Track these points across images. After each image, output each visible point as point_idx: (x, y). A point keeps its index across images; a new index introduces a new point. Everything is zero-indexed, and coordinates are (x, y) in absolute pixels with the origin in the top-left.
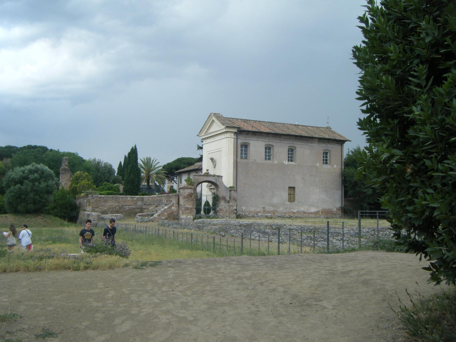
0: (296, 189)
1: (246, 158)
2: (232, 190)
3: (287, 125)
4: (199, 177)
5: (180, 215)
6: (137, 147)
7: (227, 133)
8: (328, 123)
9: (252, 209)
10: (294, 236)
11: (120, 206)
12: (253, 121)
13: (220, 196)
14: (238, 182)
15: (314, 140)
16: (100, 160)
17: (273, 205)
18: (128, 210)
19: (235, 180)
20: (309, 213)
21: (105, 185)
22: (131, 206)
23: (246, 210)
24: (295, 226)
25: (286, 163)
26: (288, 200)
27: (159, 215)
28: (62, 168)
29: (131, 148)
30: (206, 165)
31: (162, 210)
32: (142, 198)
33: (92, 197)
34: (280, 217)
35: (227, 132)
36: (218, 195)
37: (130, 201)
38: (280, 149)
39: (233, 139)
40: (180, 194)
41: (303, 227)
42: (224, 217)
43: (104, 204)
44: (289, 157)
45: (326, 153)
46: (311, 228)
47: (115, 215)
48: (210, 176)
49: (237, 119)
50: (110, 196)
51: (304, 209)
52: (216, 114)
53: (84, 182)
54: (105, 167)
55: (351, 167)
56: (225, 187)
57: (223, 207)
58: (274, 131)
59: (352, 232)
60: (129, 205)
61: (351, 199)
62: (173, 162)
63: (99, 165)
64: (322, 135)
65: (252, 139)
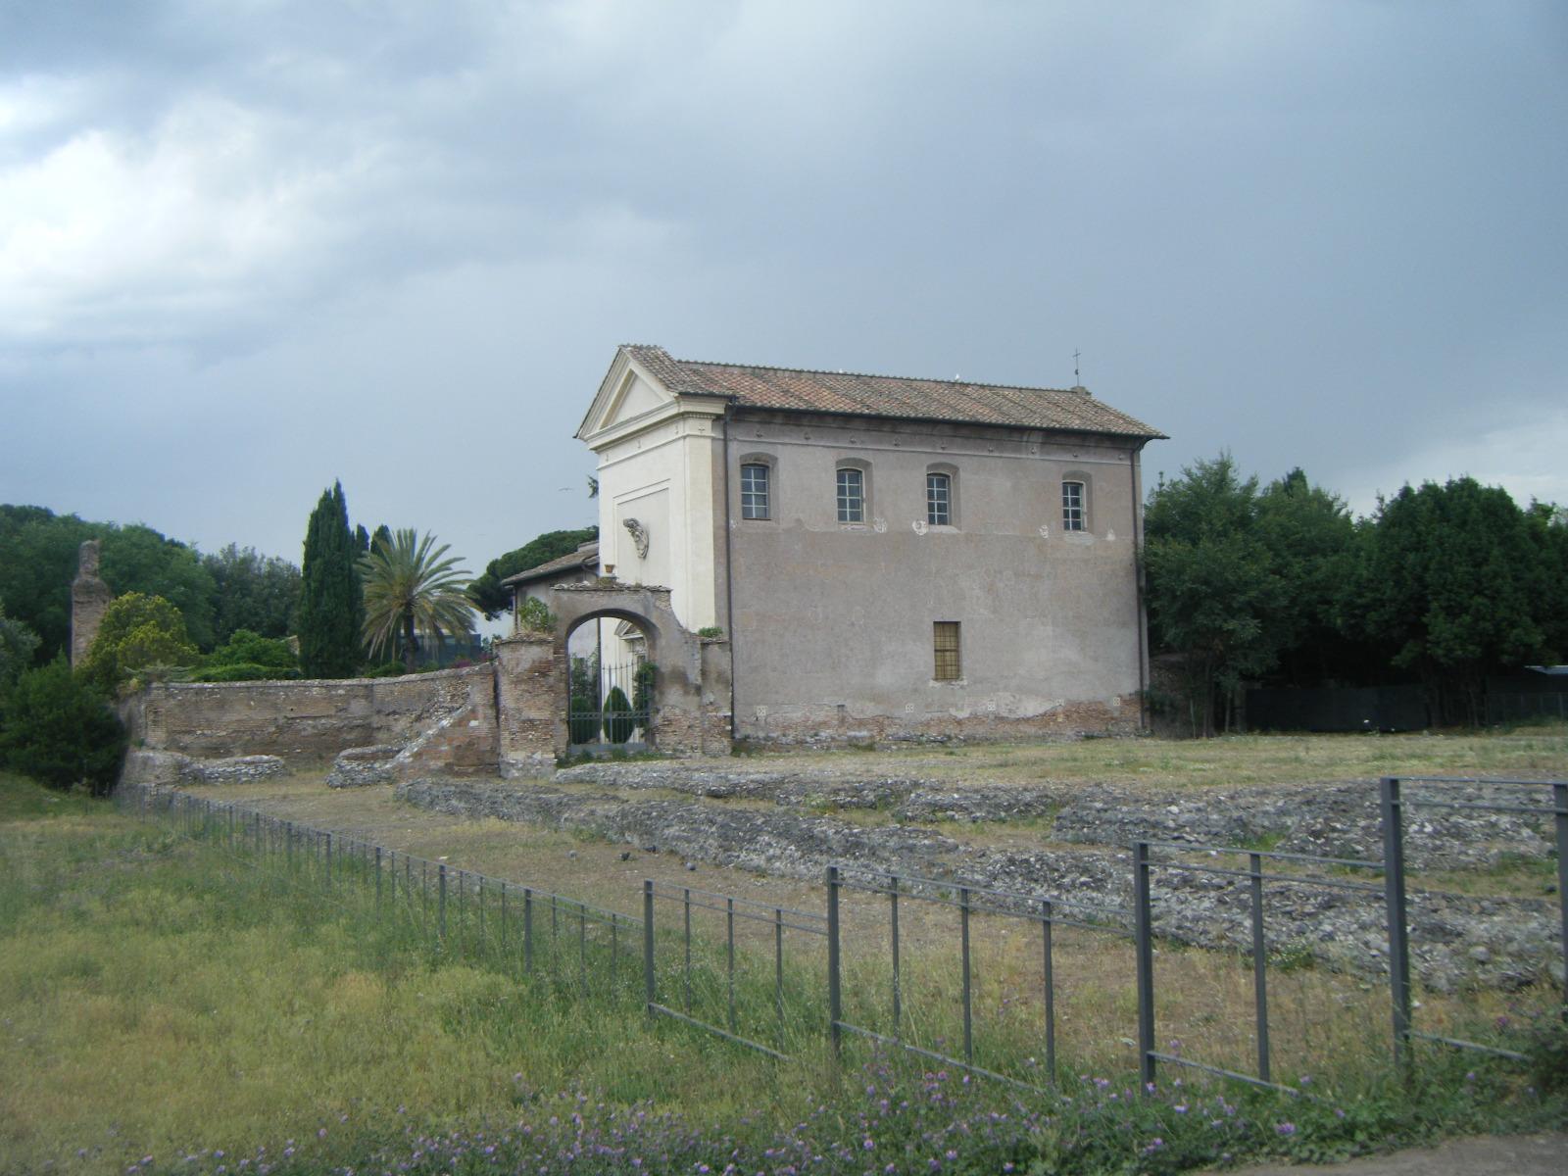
0: (963, 628)
1: (764, 516)
2: (712, 643)
3: (919, 384)
4: (577, 597)
5: (503, 750)
6: (344, 489)
7: (684, 419)
8: (1077, 373)
9: (796, 715)
10: (946, 858)
11: (282, 721)
12: (787, 374)
13: (663, 670)
14: (735, 611)
15: (1025, 439)
16: (254, 549)
17: (877, 698)
18: (316, 735)
19: (724, 603)
20: (1018, 721)
21: (239, 641)
22: (323, 721)
23: (769, 719)
24: (958, 790)
25: (922, 528)
26: (933, 674)
27: (417, 756)
28: (76, 582)
29: (321, 494)
30: (613, 551)
31: (430, 732)
32: (366, 686)
33: (167, 689)
34: (905, 739)
35: (683, 416)
36: (657, 664)
37: (316, 699)
38: (898, 478)
39: (709, 441)
40: (500, 668)
41: (991, 795)
42: (682, 751)
43: (212, 715)
44: (931, 507)
45: (1076, 489)
46: (1028, 797)
47: (248, 758)
48: (621, 589)
49: (726, 366)
50: (238, 684)
51: (998, 706)
52: (641, 348)
53: (143, 633)
54: (271, 575)
55: (1174, 536)
56: (684, 632)
57: (677, 711)
58: (869, 407)
59: (1215, 817)
60: (315, 718)
61: (1174, 658)
62: (523, 549)
63: (248, 570)
64: (1055, 418)
65: (787, 440)
